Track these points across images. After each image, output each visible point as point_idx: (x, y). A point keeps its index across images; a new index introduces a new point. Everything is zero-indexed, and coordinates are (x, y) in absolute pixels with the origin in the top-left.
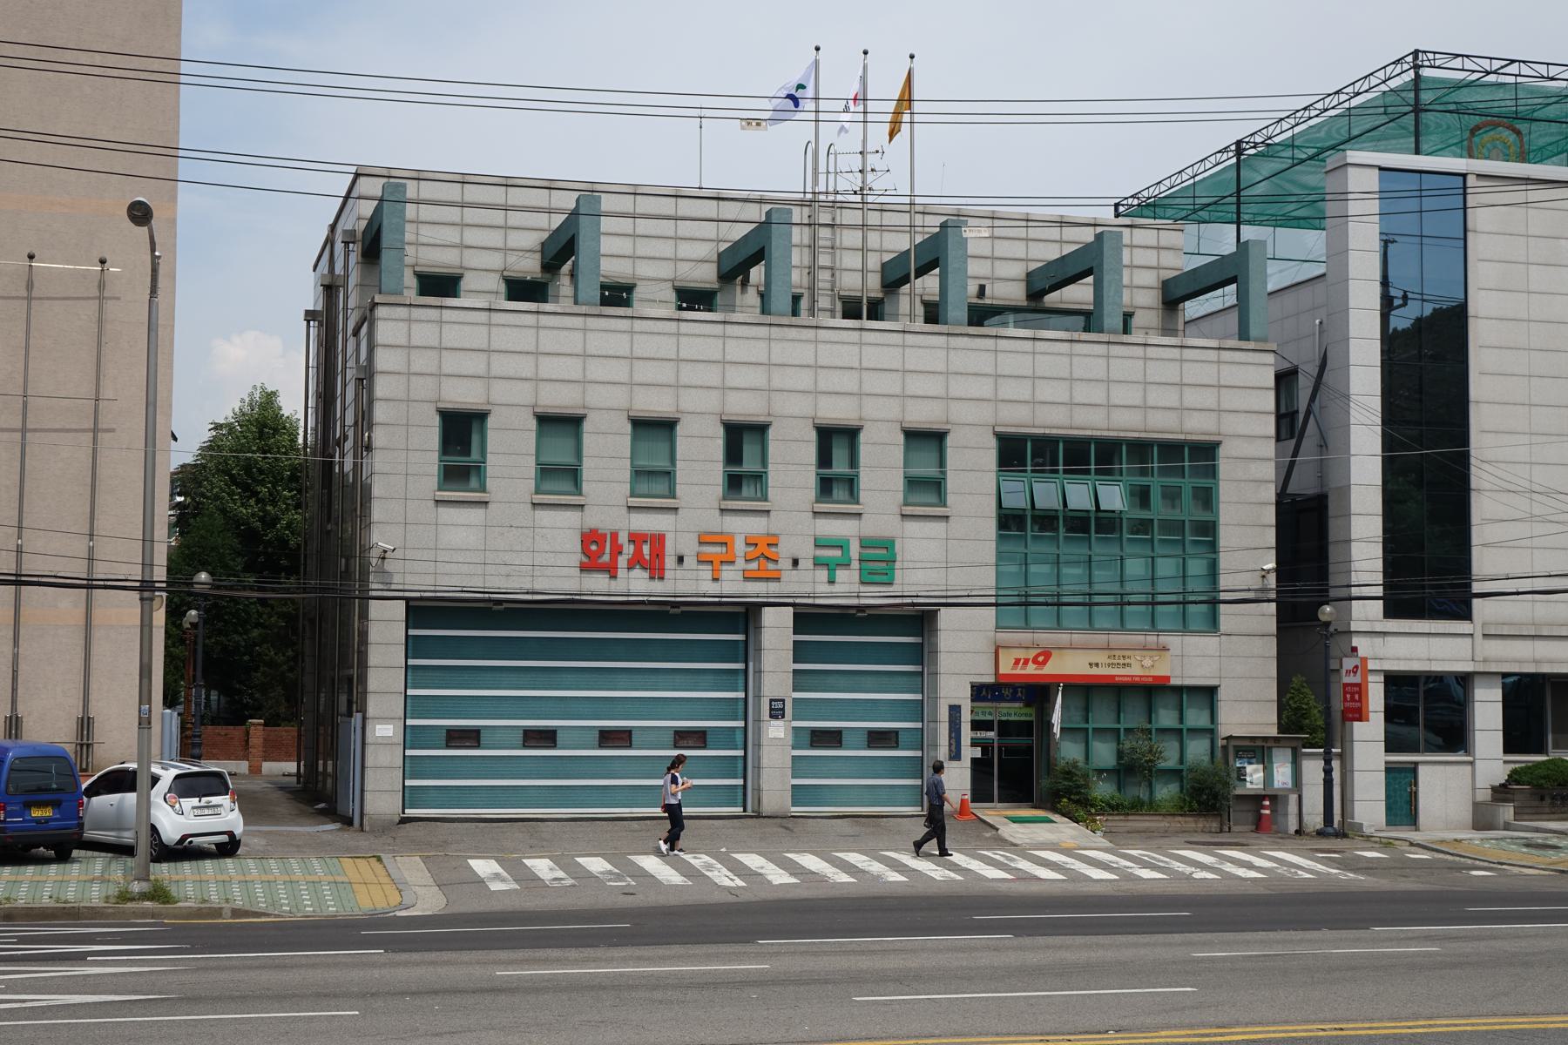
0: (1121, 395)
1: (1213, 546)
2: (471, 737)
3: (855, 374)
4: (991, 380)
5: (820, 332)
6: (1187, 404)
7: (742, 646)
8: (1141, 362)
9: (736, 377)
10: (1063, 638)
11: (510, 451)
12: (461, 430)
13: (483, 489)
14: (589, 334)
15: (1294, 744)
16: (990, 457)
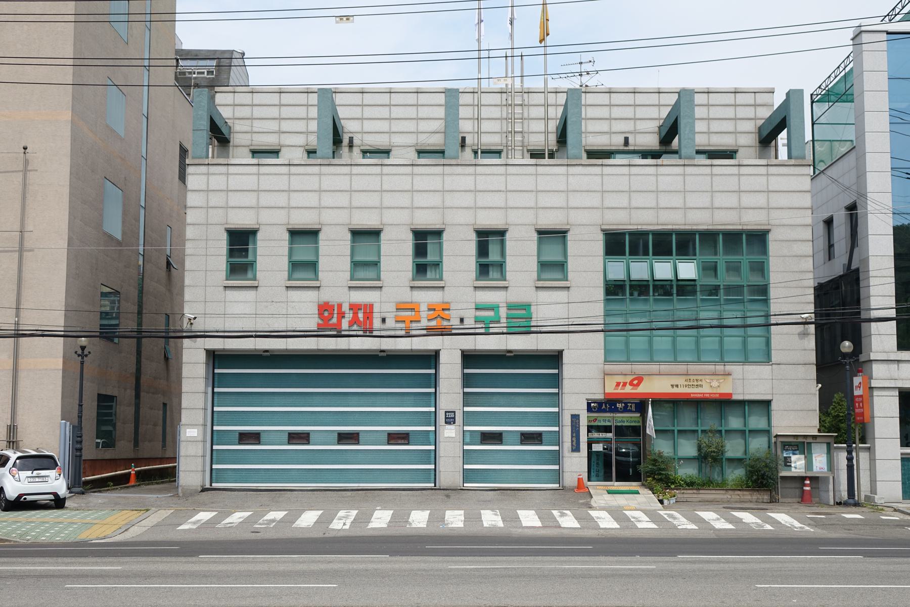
0: (694, 200)
1: (766, 302)
2: (255, 437)
3: (503, 195)
4: (599, 194)
5: (478, 168)
6: (743, 205)
7: (433, 377)
8: (709, 178)
9: (421, 200)
10: (654, 368)
11: (271, 254)
12: (240, 241)
13: (255, 279)
14: (322, 177)
15: (828, 440)
16: (599, 246)
